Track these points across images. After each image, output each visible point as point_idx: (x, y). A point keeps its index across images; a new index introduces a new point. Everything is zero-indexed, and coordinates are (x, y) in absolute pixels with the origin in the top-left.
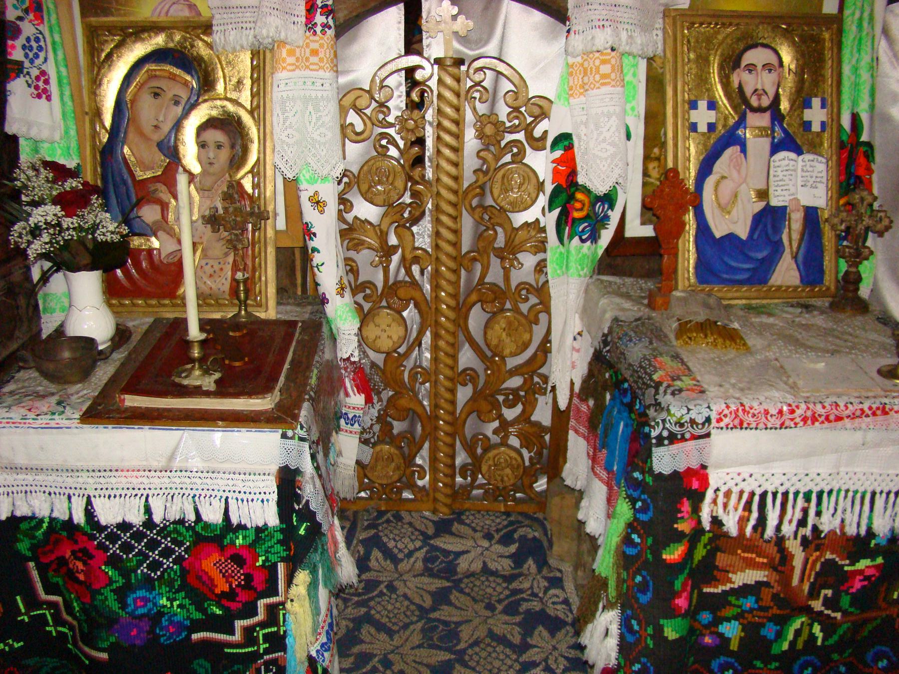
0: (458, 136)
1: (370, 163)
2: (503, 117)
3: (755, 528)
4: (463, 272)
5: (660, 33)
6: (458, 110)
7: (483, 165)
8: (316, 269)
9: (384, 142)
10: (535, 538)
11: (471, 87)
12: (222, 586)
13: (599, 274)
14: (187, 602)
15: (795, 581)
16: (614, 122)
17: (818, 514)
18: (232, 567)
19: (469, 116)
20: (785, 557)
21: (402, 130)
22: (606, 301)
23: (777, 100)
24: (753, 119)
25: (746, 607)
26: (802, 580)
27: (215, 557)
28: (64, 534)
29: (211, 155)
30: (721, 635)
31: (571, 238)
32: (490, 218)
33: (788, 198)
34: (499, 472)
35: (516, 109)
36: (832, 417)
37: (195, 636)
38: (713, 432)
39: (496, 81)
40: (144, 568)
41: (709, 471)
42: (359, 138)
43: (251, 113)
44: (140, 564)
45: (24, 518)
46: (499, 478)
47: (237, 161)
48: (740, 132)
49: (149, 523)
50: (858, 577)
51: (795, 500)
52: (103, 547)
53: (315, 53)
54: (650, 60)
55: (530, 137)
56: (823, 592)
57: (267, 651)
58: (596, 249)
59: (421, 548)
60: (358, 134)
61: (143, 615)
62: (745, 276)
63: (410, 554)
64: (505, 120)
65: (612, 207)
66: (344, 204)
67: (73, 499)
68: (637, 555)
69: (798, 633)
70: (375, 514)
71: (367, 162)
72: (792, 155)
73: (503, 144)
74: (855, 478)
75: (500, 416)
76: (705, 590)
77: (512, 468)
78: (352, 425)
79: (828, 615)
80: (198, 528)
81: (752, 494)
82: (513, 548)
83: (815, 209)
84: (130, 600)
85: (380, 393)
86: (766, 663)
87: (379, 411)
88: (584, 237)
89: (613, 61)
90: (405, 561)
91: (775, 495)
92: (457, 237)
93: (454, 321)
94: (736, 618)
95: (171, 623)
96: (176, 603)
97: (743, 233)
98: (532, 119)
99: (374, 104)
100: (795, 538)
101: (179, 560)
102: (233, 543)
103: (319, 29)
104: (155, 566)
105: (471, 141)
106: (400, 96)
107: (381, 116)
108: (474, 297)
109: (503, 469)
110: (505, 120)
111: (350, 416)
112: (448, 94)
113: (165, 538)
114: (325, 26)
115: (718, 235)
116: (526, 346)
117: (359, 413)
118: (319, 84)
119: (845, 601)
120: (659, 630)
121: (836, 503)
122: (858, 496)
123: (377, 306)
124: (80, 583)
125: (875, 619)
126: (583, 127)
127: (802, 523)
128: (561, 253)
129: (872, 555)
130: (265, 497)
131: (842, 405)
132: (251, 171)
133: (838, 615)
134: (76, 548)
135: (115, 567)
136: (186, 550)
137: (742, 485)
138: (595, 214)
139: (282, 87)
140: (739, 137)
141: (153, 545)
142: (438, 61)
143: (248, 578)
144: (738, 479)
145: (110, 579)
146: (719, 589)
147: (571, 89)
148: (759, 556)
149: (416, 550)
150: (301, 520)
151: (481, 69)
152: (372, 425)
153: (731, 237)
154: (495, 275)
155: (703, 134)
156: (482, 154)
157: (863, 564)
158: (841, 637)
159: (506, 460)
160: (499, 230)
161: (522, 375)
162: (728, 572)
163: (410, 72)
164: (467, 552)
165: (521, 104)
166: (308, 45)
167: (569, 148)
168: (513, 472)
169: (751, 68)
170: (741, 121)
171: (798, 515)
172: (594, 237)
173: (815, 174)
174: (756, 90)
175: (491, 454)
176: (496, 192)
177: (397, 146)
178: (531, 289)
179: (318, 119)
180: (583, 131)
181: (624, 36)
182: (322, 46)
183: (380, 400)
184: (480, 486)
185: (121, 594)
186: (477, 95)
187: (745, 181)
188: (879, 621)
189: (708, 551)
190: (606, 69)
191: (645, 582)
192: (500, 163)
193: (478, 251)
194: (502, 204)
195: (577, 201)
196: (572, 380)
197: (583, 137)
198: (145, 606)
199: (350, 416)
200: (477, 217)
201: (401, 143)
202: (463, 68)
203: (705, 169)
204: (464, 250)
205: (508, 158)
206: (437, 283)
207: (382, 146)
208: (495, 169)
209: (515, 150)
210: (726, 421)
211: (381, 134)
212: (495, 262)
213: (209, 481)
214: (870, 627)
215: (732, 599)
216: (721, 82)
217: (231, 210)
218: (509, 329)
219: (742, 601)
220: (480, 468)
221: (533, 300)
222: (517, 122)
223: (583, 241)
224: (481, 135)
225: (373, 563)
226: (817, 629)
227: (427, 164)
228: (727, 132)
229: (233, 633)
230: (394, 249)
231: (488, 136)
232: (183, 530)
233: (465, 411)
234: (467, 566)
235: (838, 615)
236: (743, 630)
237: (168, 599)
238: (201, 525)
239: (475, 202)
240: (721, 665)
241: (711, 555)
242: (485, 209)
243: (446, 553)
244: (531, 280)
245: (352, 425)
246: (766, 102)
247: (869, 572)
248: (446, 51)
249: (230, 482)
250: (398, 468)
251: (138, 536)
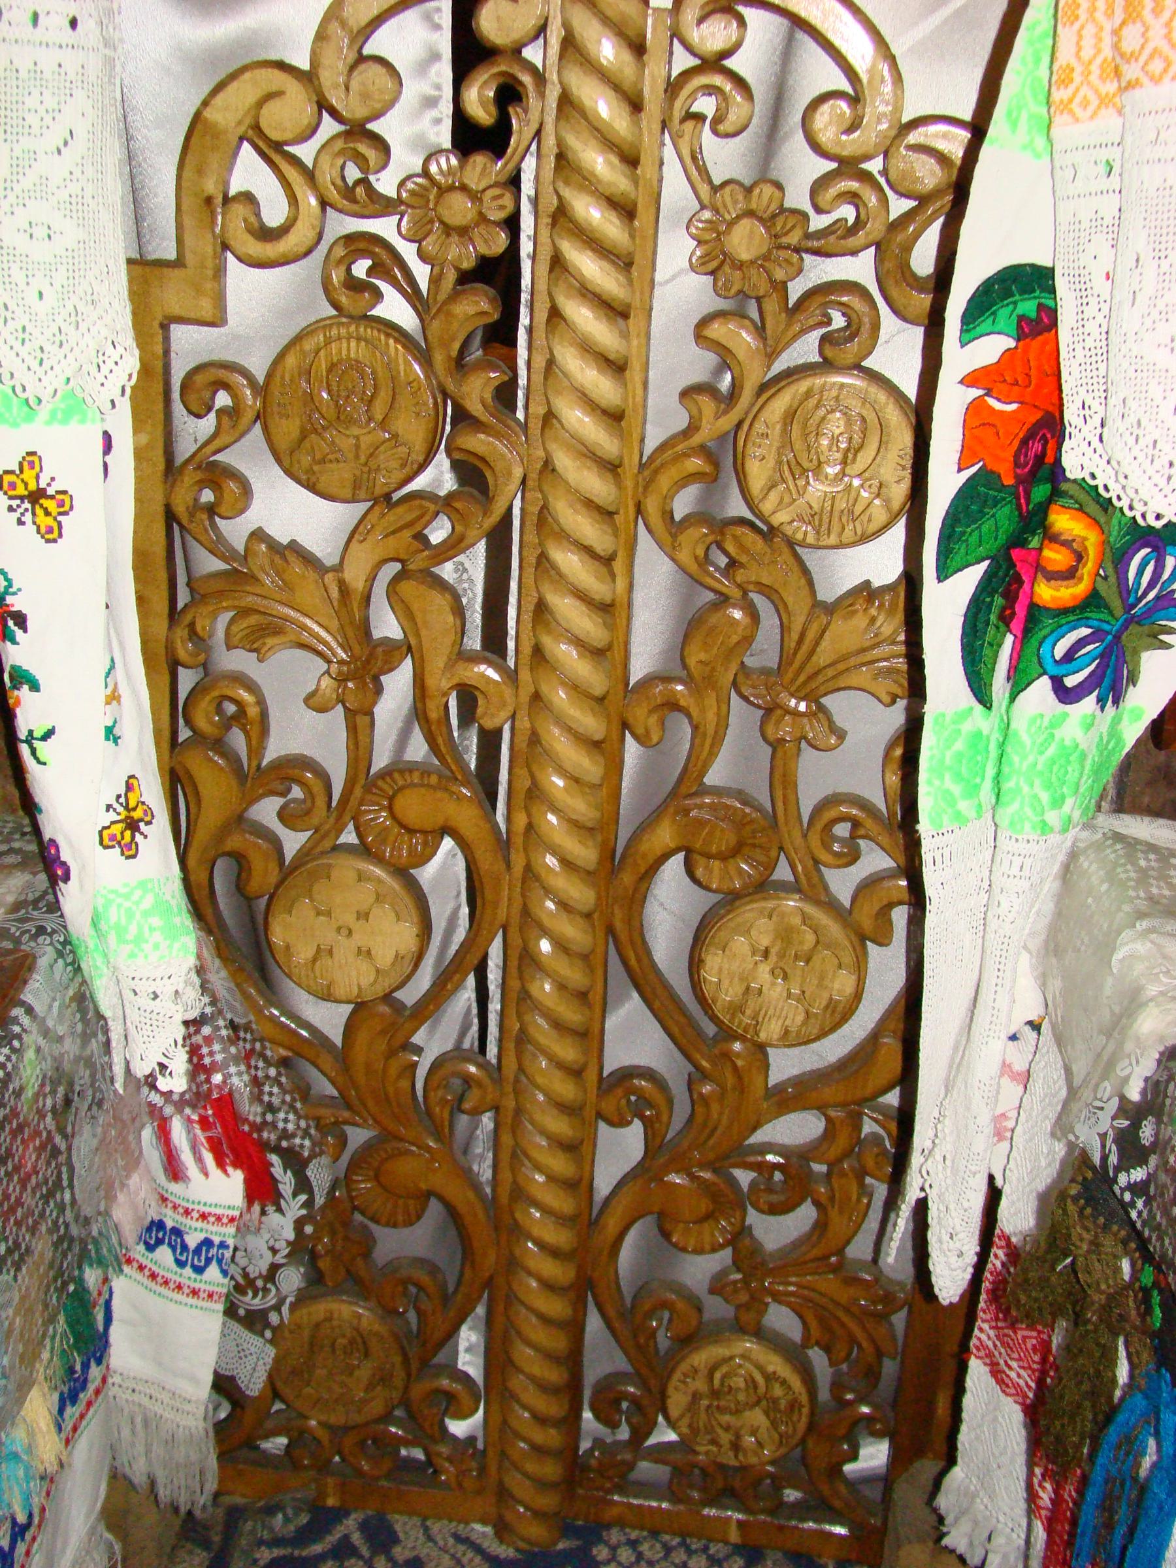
1: (308, 345)
2: (798, 197)
4: (632, 750)
6: (631, 160)
8: (24, 749)
11: (687, 74)
13: (1120, 807)
22: (1141, 947)
31: (1018, 682)
32: (733, 564)
34: (726, 1418)
39: (787, 55)
46: (725, 1438)
58: (1116, 721)
64: (807, 207)
66: (216, 487)
70: (304, 1519)
71: (298, 339)
73: (796, 290)
75: (740, 1237)
77: (771, 1406)
78: (199, 1270)
85: (305, 1163)
87: (299, 1224)
88: (1071, 681)
92: (610, 627)
93: (588, 916)
98: (909, 204)
99: (329, 127)
106: (430, 102)
108: (664, 835)
110: (807, 207)
111: (192, 1241)
116: (841, 1014)
117: (225, 1233)
123: (327, 844)
126: (1101, 244)
128: (979, 734)
138: (1124, 590)
152: (274, 1268)
156: (716, 330)
159: (752, 1383)
161: (821, 1108)
165: (869, 148)
168: (774, 1424)
175: (701, 1358)
176: (758, 473)
178: (869, 823)
183: (303, 1185)
186: (706, 105)
192: (779, 366)
194: (779, 519)
195: (1052, 538)
196: (991, 1178)
197: (1100, 286)
199: (192, 1241)
200: (684, 556)
201: (422, 273)
206: (535, 783)
207: (354, 285)
208: (763, 388)
211: (350, 239)
218: (782, 956)
220: (663, 1396)
222: (847, 212)
223: (1065, 694)
230: (391, 653)
231: (740, 266)
239: (683, 504)
242: (722, 527)
245: (199, 1270)
250: (382, 1378)
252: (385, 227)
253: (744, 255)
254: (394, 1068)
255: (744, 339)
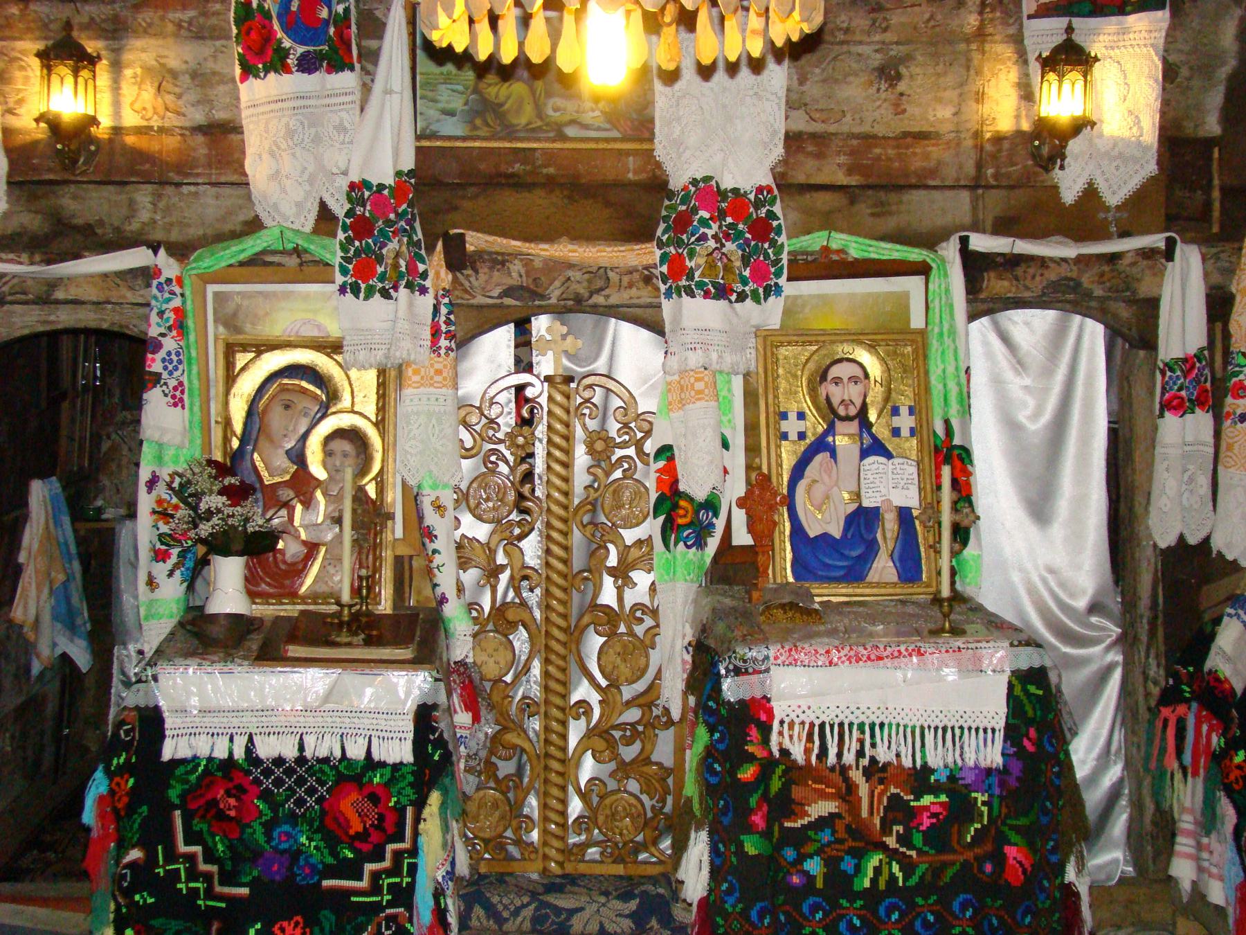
0: (568, 452)
2: (613, 434)
3: (818, 757)
5: (753, 351)
6: (567, 425)
7: (595, 481)
9: (493, 458)
10: (658, 895)
11: (581, 404)
12: (357, 826)
14: (322, 844)
15: (865, 813)
16: (709, 433)
17: (873, 745)
18: (368, 804)
19: (579, 433)
20: (851, 788)
21: (513, 445)
23: (864, 409)
24: (839, 426)
25: (825, 841)
26: (871, 813)
27: (354, 796)
28: (220, 774)
29: (338, 463)
30: (806, 873)
31: (676, 544)
33: (879, 499)
35: (626, 425)
36: (873, 657)
37: (326, 883)
38: (772, 667)
39: (606, 398)
40: (290, 804)
41: (773, 703)
42: (468, 454)
43: (376, 425)
44: (287, 800)
45: (183, 761)
47: (363, 470)
48: (830, 439)
49: (301, 760)
50: (925, 814)
51: (851, 732)
52: (257, 782)
53: (439, 372)
54: (747, 376)
55: (640, 452)
56: (895, 828)
57: (391, 904)
58: (703, 556)
59: (528, 904)
60: (467, 450)
61: (285, 851)
62: (842, 573)
63: (516, 913)
65: (716, 515)
67: (236, 738)
68: (719, 782)
69: (877, 870)
71: (476, 478)
72: (882, 459)
73: (614, 459)
74: (903, 714)
76: (787, 824)
79: (903, 853)
80: (341, 768)
81: (812, 725)
82: (633, 905)
83: (909, 509)
84: (275, 834)
86: (851, 901)
89: (706, 379)
90: (511, 922)
91: (832, 726)
94: (818, 852)
95: (307, 863)
96: (313, 844)
97: (837, 533)
99: (484, 421)
100: (857, 768)
101: (320, 800)
102: (371, 781)
103: (443, 351)
104: (300, 802)
105: (581, 457)
107: (491, 433)
108: (586, 619)
109: (622, 819)
112: (558, 411)
113: (311, 776)
114: (449, 349)
115: (812, 534)
118: (433, 399)
119: (918, 839)
120: (740, 845)
121: (890, 736)
122: (909, 730)
124: (231, 819)
125: (953, 863)
127: (860, 754)
129: (935, 790)
130: (403, 736)
131: (882, 647)
132: (375, 478)
133: (913, 853)
134: (231, 785)
135: (266, 801)
136: (327, 791)
137: (802, 717)
139: (408, 402)
140: (828, 444)
141: (301, 781)
142: (548, 379)
143: (381, 818)
144: (799, 712)
145: (261, 812)
146: (798, 824)
147: (670, 403)
148: (827, 786)
149: (524, 906)
150: (435, 749)
151: (590, 386)
153: (825, 537)
154: (608, 595)
155: (793, 442)
157: (927, 800)
158: (922, 878)
159: (625, 809)
160: (611, 547)
162: (804, 805)
163: (520, 389)
164: (582, 909)
166: (432, 365)
167: (671, 459)
169: (837, 381)
170: (831, 430)
171: (855, 746)
172: (700, 544)
173: (905, 477)
174: (843, 401)
175: (607, 801)
177: (507, 462)
179: (441, 431)
180: (682, 442)
181: (714, 356)
182: (445, 366)
184: (597, 844)
185: (269, 827)
186: (586, 411)
187: (836, 484)
188: (957, 866)
189: (783, 784)
190: (700, 386)
191: (726, 806)
193: (589, 571)
198: (287, 840)
201: (511, 458)
202: (573, 385)
203: (798, 471)
204: (575, 570)
205: (618, 474)
207: (492, 463)
209: (626, 466)
210: (782, 658)
212: (608, 581)
213: (356, 720)
214: (950, 872)
215: (811, 833)
216: (809, 394)
217: (359, 511)
219: (820, 835)
221: (649, 622)
222: (627, 437)
223: (688, 547)
224: (591, 451)
225: (474, 923)
226: (895, 868)
227: (537, 481)
228: (817, 439)
229: (360, 879)
230: (502, 568)
232: (326, 768)
233: (579, 749)
234: (581, 928)
235: (913, 853)
236: (825, 865)
237: (308, 838)
238: (345, 763)
239: (586, 519)
240: (811, 906)
241: (786, 788)
243: (558, 910)
244: (646, 601)
246: (853, 411)
247: (937, 809)
248: (556, 369)
249: (375, 722)
251: (290, 772)
252: (501, 447)
253: (599, 449)
254: (506, 702)
255: (599, 472)
